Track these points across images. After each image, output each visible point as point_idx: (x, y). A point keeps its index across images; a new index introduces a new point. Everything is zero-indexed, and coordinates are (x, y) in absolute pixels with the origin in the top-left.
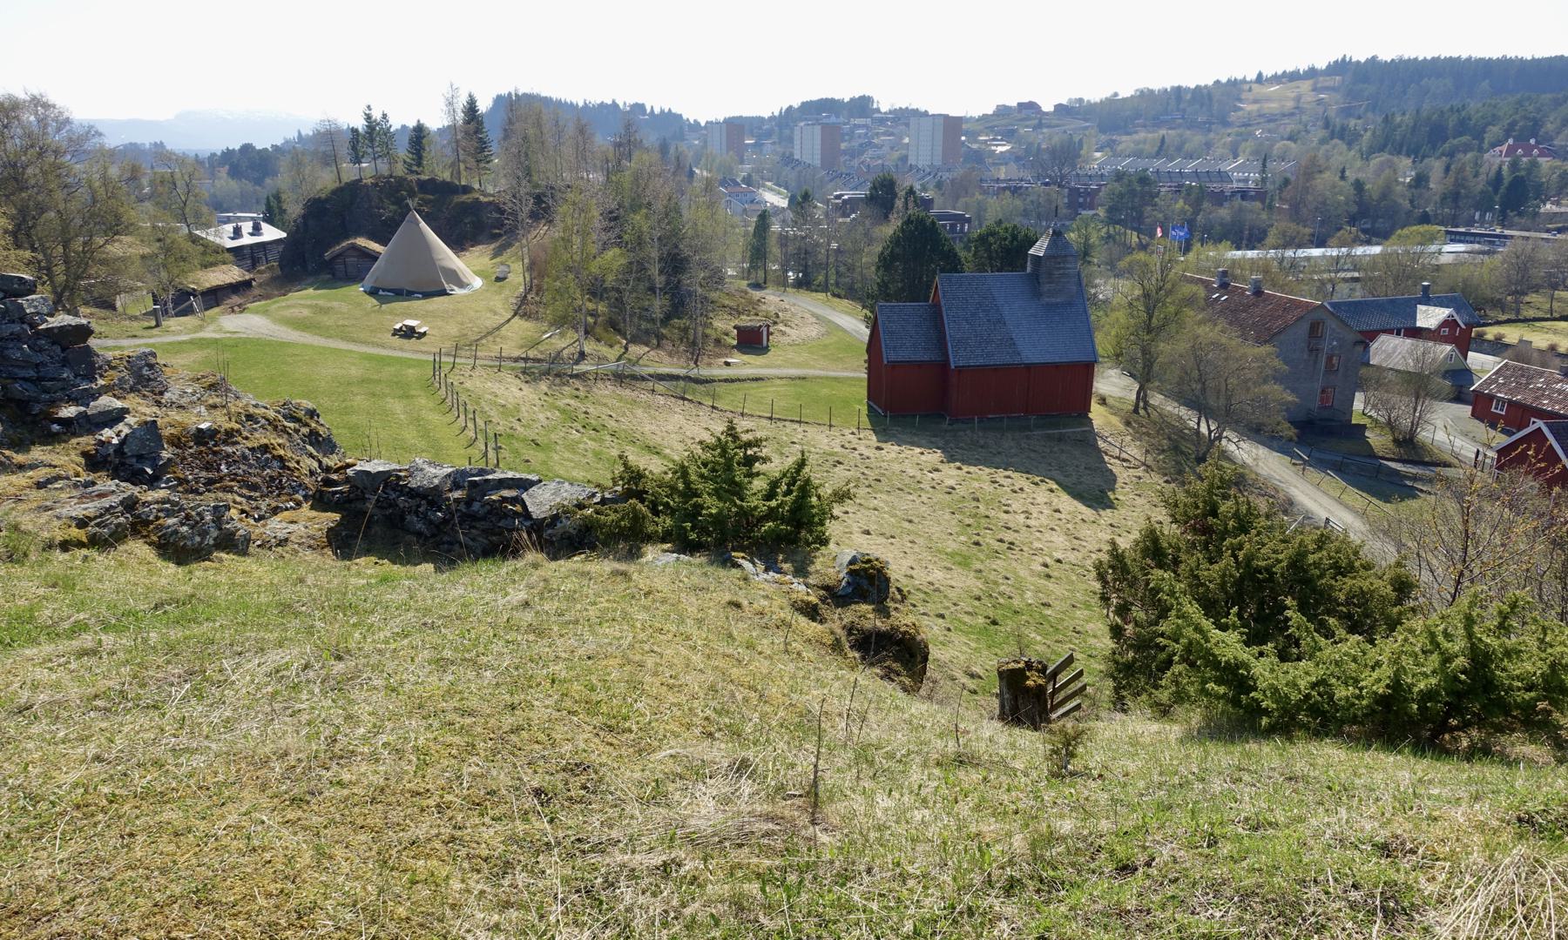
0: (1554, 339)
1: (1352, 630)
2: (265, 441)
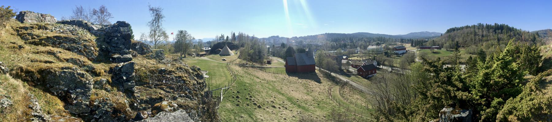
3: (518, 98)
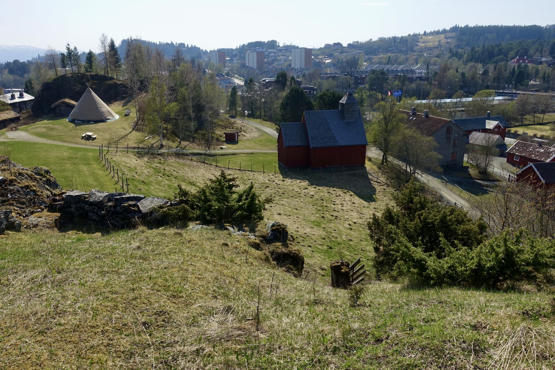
0: (536, 132)
1: (464, 245)
2: (27, 184)
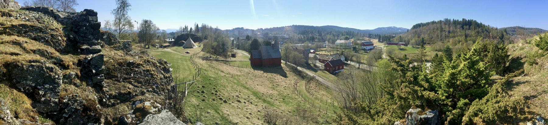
2: (148, 68)
3: (484, 100)
